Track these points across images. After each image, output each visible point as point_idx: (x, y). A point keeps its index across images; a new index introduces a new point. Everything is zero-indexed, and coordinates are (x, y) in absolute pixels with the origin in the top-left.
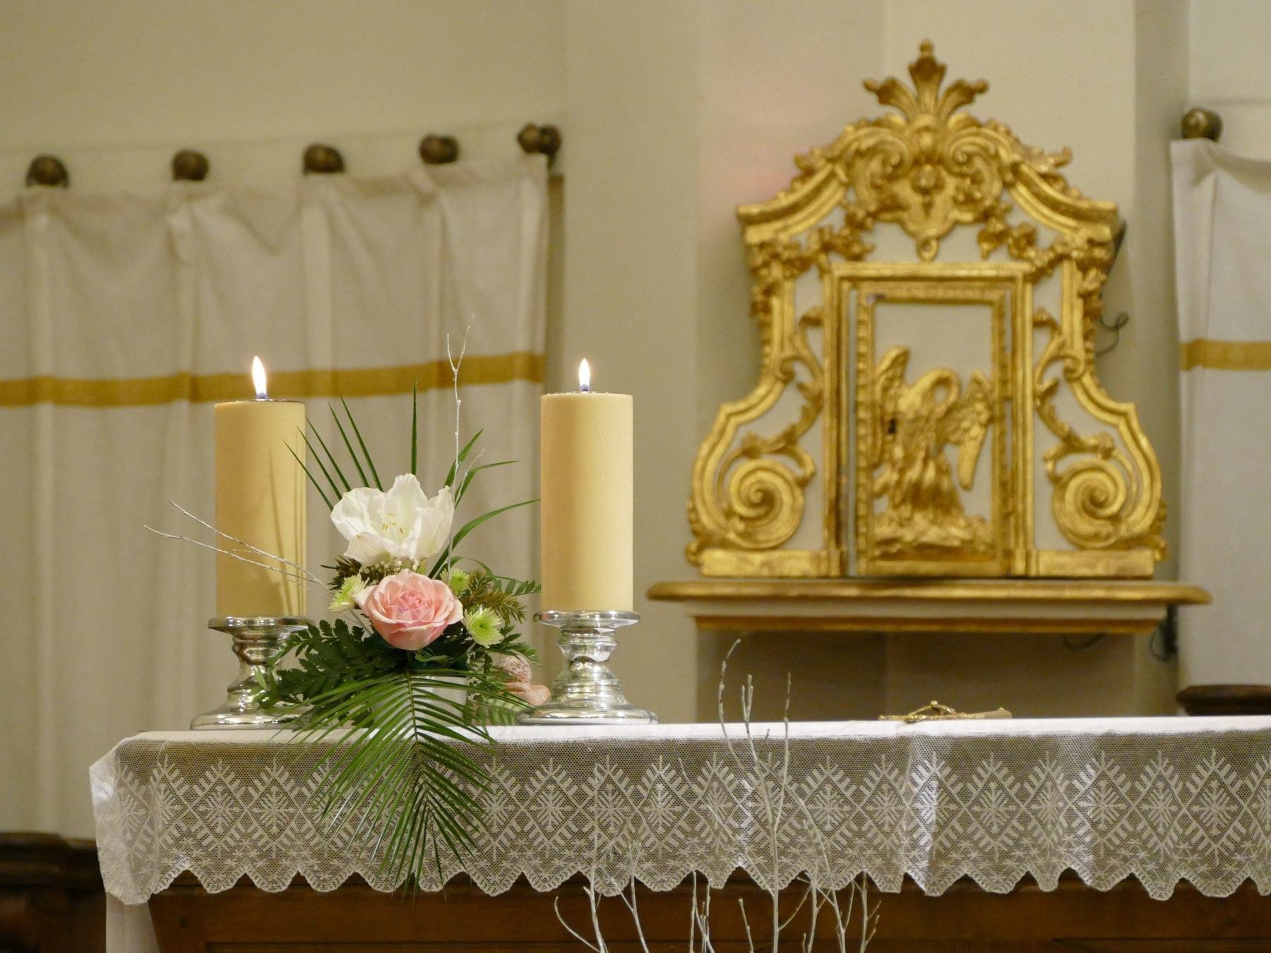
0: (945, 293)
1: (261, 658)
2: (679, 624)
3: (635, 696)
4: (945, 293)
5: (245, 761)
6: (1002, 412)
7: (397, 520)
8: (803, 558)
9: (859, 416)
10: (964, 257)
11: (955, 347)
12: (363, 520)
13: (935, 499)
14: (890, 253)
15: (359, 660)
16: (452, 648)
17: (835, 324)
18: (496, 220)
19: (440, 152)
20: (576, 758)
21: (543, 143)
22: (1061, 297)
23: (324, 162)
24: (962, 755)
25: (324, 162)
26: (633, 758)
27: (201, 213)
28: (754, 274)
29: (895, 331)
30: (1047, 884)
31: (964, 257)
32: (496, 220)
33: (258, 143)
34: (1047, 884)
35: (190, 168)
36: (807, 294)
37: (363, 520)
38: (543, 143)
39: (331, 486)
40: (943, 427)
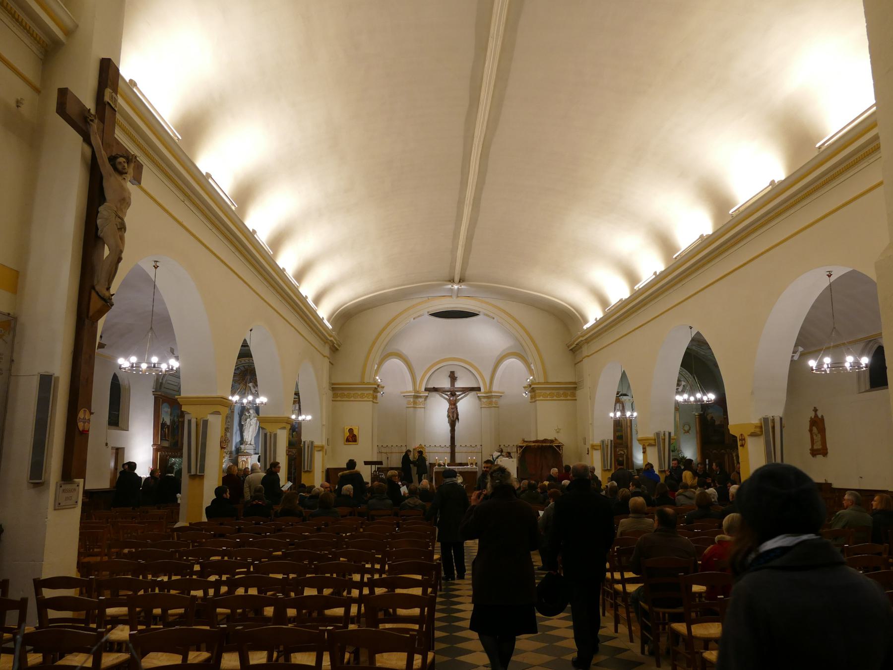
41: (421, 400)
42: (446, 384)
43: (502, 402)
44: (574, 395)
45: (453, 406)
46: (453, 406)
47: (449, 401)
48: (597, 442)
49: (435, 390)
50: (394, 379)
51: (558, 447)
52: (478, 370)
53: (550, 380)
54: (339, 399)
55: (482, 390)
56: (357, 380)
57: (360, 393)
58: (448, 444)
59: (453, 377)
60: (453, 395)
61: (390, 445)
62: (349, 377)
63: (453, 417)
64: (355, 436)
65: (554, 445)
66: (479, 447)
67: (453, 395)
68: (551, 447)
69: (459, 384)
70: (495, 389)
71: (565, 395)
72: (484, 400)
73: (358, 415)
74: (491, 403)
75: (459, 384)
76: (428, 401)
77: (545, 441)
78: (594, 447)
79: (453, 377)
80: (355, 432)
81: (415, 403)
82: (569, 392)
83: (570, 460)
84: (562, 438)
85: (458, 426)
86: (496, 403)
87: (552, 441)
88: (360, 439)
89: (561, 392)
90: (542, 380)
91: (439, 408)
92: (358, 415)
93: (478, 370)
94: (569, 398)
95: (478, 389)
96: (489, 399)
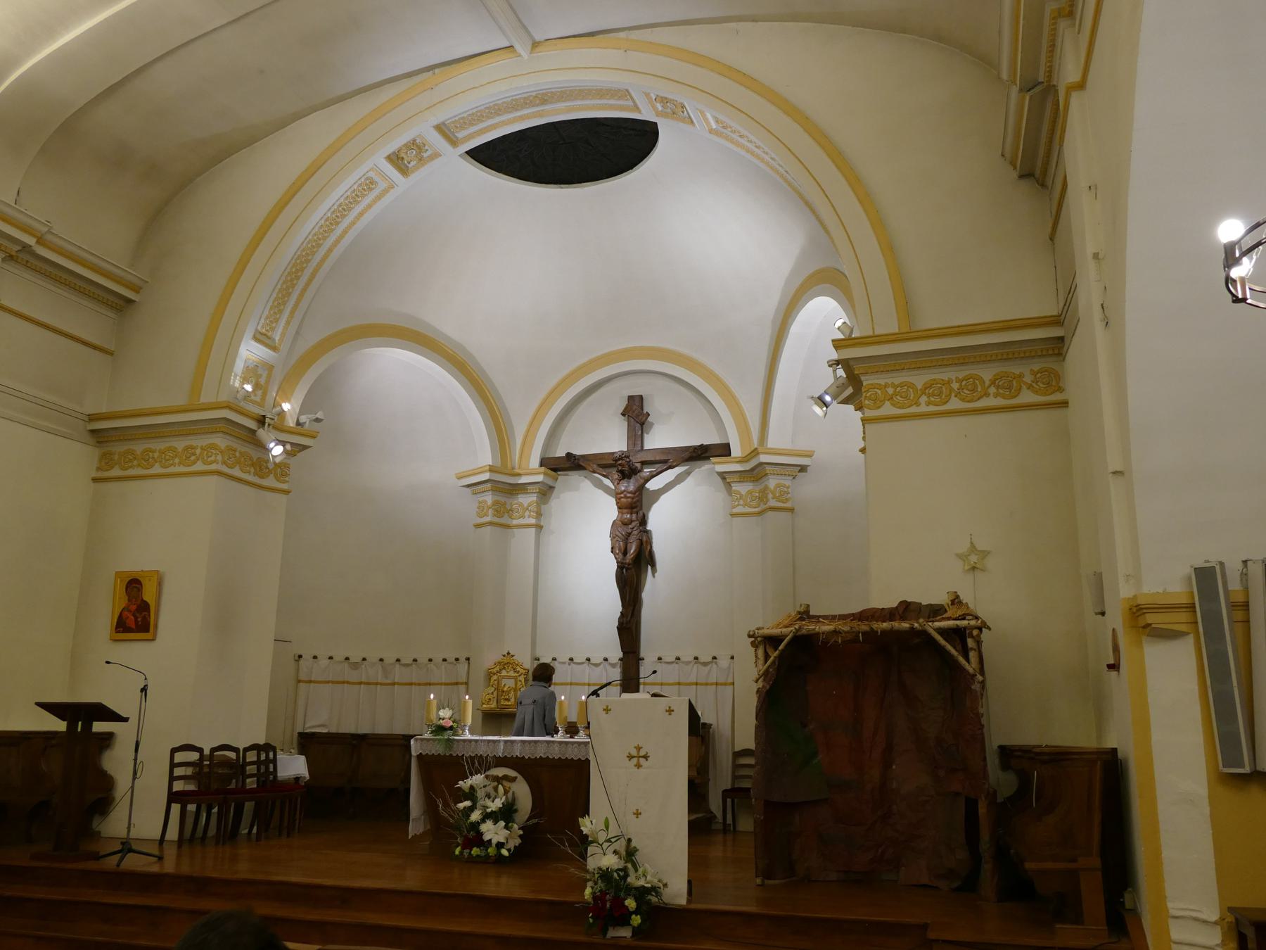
0: (509, 677)
1: (533, 521)
2: (480, 713)
3: (472, 733)
4: (509, 677)
5: (428, 740)
6: (515, 690)
7: (445, 713)
8: (493, 705)
9: (500, 691)
10: (512, 673)
11: (511, 683)
12: (442, 713)
13: (508, 700)
14: (504, 673)
15: (440, 729)
16: (451, 728)
17: (498, 681)
18: (463, 667)
19: (457, 659)
20: (464, 741)
21: (468, 659)
22: (522, 678)
23: (445, 660)
24: (506, 742)
25: (445, 660)
26: (470, 741)
27: (431, 665)
28: (489, 675)
29: (504, 681)
30: (521, 832)
31: (512, 673)
32: (463, 667)
33: (438, 657)
34: (521, 832)
35: (430, 660)
36: (495, 677)
37: (442, 713)
38: (468, 659)
39: (439, 709)
40: (509, 692)
41: (528, 500)
42: (613, 440)
43: (805, 491)
44: (1053, 381)
45: (634, 509)
46: (634, 509)
47: (617, 496)
48: (1166, 579)
49: (574, 463)
50: (419, 427)
51: (958, 635)
52: (710, 376)
53: (930, 321)
54: (116, 472)
55: (736, 451)
56: (180, 400)
57: (180, 444)
58: (616, 653)
59: (636, 414)
60: (629, 473)
61: (687, 656)
62: (149, 390)
63: (634, 563)
64: (144, 607)
65: (933, 627)
66: (724, 662)
67: (629, 473)
68: (924, 634)
69: (659, 439)
70: (773, 441)
71: (1007, 385)
72: (743, 488)
73: (175, 524)
74: (763, 497)
75: (659, 439)
76: (555, 503)
77: (906, 610)
78: (1145, 620)
79: (636, 414)
80: (148, 595)
81: (501, 510)
82: (1026, 370)
83: (1026, 709)
84: (1005, 606)
85: (654, 588)
86: (783, 495)
87: (936, 611)
88: (167, 619)
89: (986, 373)
90: (906, 330)
91: (586, 522)
92: (175, 524)
93: (710, 376)
94: (1027, 397)
95: (723, 450)
96: (758, 479)
